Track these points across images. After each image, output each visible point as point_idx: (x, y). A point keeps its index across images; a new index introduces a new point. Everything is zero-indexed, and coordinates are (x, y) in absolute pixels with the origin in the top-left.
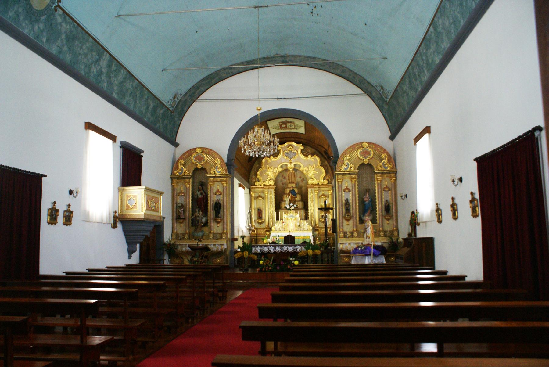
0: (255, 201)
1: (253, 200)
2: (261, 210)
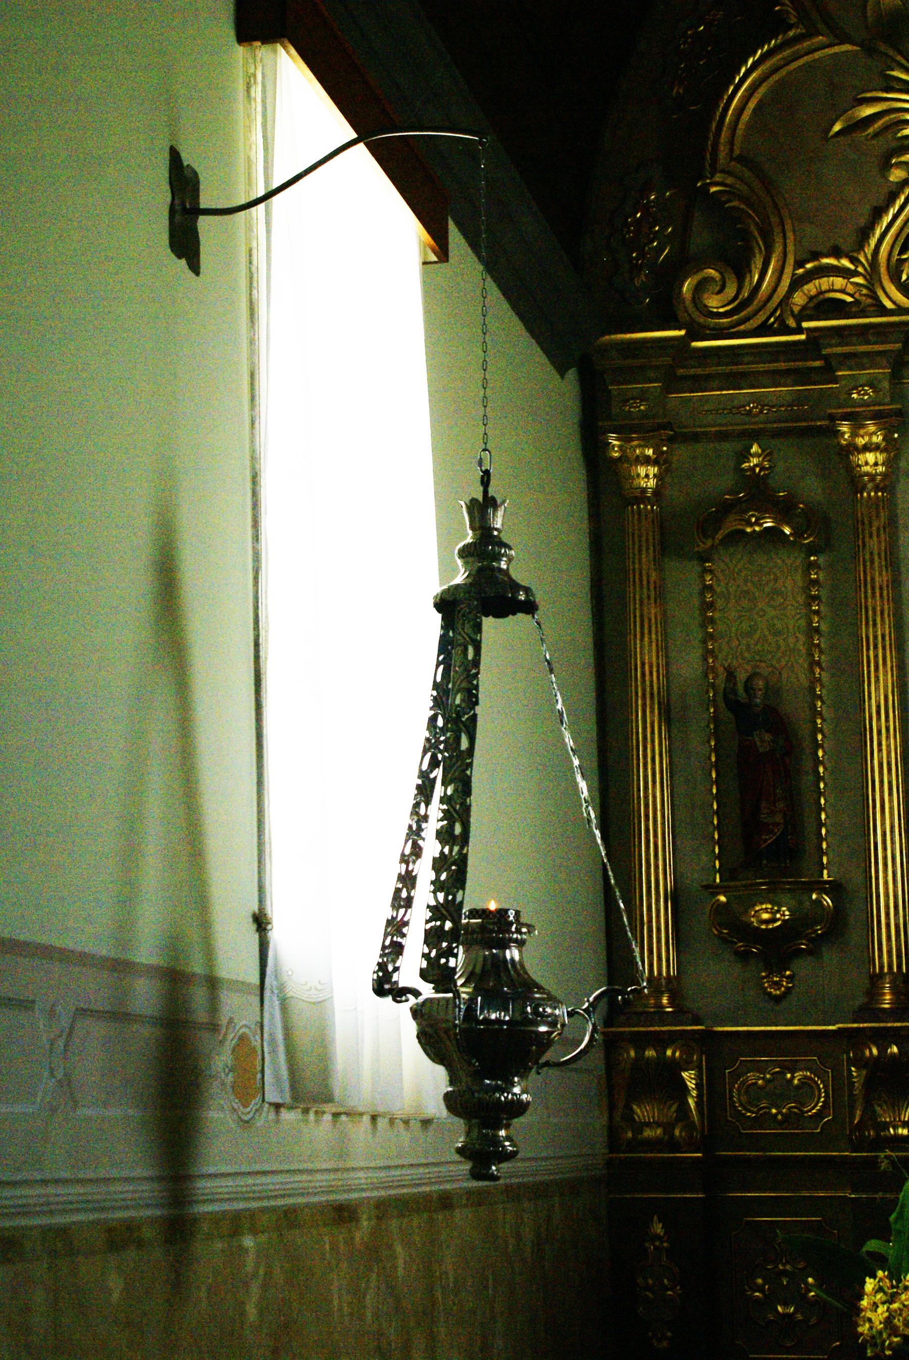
0: (684, 576)
1: (643, 561)
2: (775, 720)
